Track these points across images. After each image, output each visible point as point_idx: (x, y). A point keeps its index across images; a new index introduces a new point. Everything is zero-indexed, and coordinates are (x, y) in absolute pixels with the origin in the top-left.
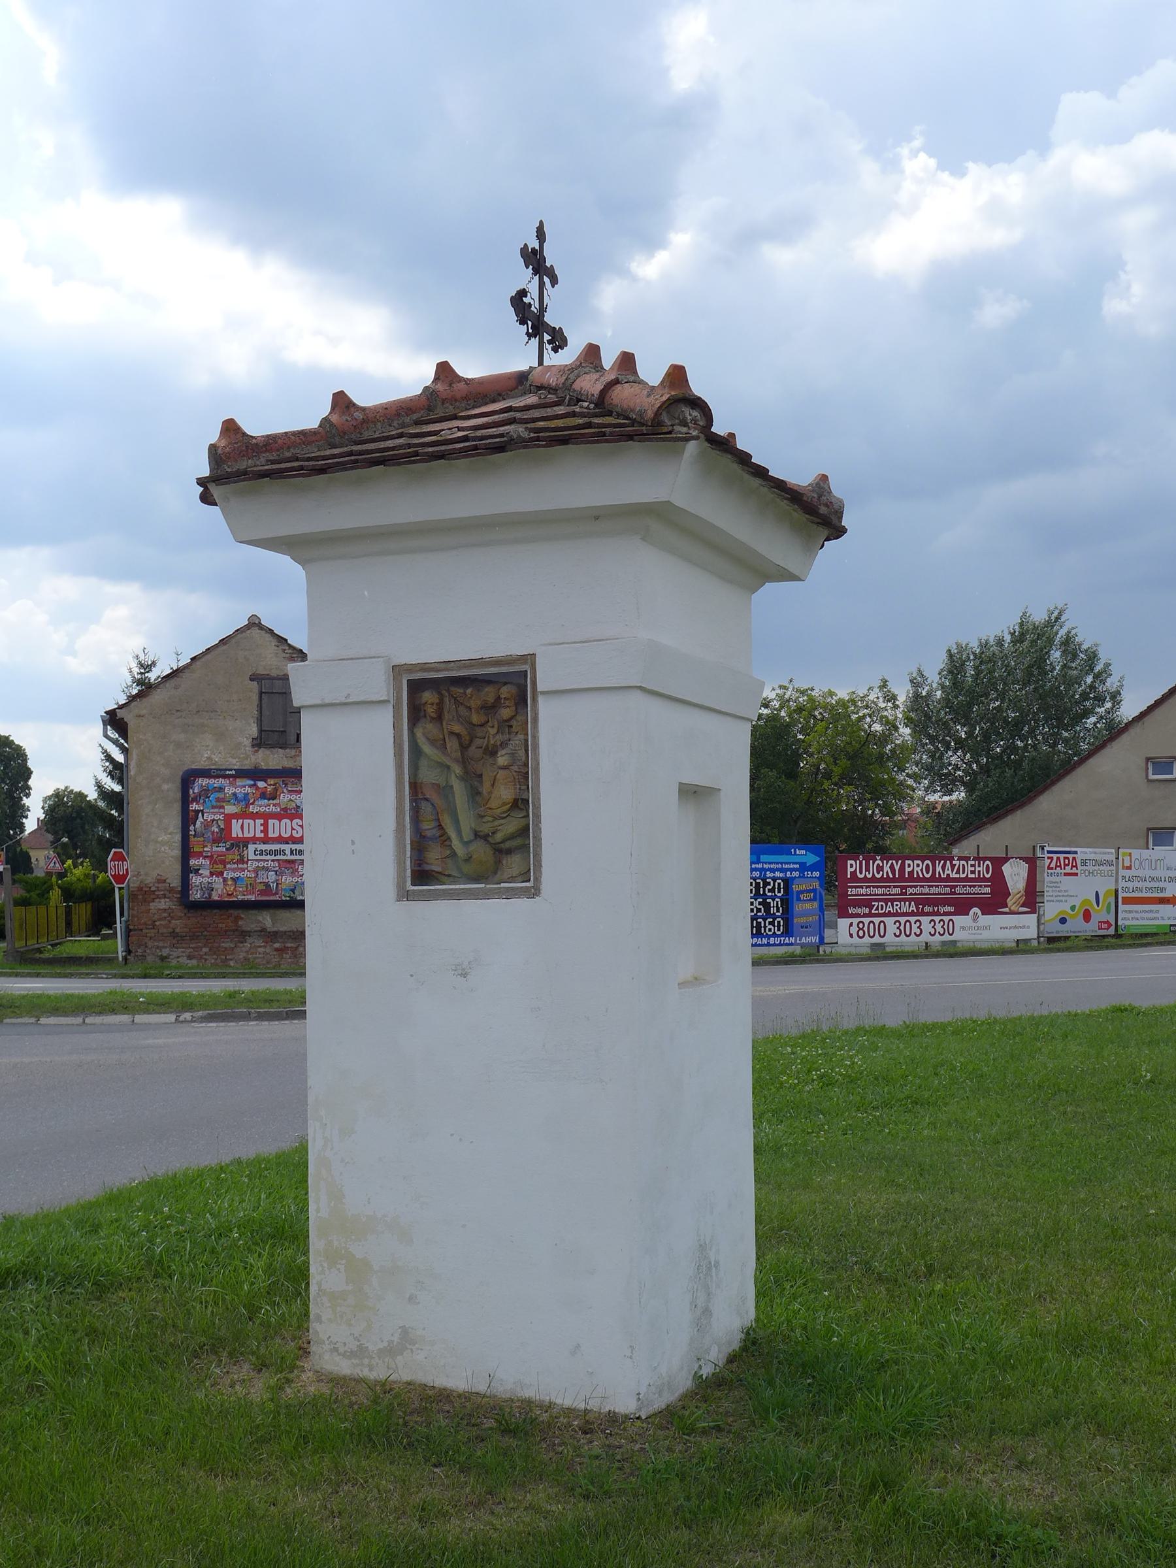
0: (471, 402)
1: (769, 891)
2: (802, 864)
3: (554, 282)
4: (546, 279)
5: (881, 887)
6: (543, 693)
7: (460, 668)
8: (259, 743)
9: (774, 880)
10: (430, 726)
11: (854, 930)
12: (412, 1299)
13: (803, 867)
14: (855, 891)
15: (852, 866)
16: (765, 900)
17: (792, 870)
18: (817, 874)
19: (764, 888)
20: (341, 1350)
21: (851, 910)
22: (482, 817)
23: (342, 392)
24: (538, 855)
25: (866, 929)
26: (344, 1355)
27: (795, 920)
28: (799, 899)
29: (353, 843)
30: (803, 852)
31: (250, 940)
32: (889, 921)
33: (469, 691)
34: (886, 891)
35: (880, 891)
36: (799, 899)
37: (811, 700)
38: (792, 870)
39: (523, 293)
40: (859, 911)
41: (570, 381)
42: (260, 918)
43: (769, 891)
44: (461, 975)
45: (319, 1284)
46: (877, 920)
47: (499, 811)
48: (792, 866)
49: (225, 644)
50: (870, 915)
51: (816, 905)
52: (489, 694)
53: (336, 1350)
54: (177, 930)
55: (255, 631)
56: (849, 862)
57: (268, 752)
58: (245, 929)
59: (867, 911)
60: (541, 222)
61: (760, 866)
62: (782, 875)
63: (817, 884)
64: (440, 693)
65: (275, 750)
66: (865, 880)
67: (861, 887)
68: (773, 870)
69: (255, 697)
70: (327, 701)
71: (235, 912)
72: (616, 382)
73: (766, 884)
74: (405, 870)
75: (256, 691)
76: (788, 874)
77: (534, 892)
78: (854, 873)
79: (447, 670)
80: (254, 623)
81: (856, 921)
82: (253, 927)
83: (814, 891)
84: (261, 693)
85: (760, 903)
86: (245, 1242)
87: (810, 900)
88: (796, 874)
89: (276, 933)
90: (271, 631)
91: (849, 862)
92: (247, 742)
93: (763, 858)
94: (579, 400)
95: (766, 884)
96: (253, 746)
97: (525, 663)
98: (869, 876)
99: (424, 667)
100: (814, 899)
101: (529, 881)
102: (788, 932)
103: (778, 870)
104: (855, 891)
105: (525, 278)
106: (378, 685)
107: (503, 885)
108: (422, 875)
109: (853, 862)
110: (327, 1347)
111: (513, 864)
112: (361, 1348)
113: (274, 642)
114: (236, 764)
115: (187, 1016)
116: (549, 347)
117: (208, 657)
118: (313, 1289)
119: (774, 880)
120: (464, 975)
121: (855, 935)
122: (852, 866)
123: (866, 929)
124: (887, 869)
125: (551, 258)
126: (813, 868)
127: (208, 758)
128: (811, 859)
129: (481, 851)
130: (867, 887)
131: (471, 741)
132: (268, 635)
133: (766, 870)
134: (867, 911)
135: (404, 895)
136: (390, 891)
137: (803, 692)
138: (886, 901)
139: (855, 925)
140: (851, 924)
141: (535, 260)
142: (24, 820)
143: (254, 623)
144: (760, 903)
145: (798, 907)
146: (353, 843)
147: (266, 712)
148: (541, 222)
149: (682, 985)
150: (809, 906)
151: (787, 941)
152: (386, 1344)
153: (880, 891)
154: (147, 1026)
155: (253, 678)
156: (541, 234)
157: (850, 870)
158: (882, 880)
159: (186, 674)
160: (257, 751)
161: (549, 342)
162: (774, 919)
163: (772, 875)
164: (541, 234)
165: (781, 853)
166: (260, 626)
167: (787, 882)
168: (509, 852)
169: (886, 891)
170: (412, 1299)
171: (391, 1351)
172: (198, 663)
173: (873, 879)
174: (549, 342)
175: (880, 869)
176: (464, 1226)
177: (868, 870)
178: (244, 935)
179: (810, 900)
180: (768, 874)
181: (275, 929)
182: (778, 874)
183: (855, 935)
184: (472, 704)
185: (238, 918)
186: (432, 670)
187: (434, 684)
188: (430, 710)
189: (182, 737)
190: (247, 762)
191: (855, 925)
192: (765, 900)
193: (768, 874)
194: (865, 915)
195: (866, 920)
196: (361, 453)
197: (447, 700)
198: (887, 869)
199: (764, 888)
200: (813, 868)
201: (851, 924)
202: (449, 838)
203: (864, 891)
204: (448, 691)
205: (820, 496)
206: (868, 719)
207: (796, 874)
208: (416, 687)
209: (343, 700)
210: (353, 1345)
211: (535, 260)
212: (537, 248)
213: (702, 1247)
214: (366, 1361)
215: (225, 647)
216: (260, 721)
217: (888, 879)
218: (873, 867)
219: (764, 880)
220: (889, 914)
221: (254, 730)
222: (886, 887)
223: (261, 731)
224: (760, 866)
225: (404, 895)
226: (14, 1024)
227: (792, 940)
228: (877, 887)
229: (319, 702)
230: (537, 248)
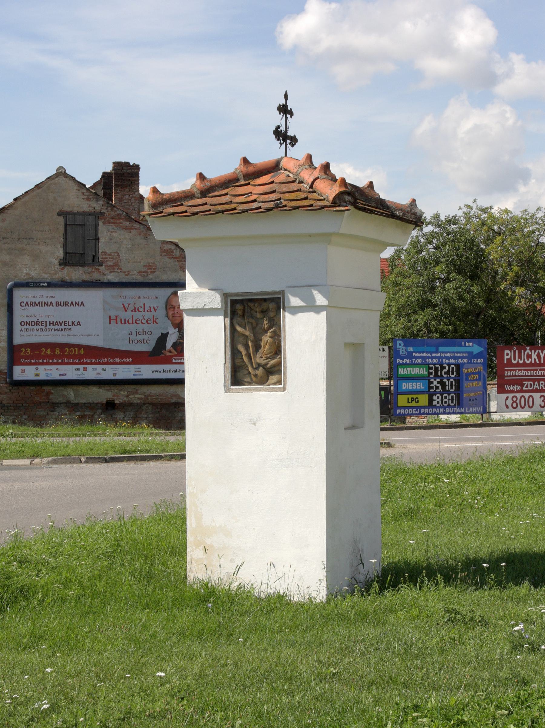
0: (256, 176)
1: (445, 373)
2: (470, 353)
3: (291, 114)
4: (289, 116)
5: (530, 370)
8: (65, 263)
9: (449, 365)
10: (239, 319)
11: (509, 402)
13: (471, 356)
14: (510, 373)
15: (508, 355)
16: (442, 380)
17: (462, 358)
18: (481, 361)
19: (441, 371)
21: (507, 388)
24: (285, 374)
25: (518, 402)
27: (465, 395)
28: (467, 379)
29: (206, 368)
30: (471, 344)
31: (58, 410)
32: (537, 396)
33: (256, 305)
34: (533, 373)
35: (529, 373)
36: (467, 379)
37: (491, 216)
38: (462, 358)
39: (278, 127)
40: (513, 388)
41: (299, 172)
42: (65, 393)
43: (445, 373)
45: (191, 556)
46: (527, 395)
48: (462, 355)
49: (39, 189)
50: (521, 391)
51: (480, 383)
52: (265, 306)
54: (4, 402)
55: (61, 179)
56: (506, 352)
57: (71, 269)
58: (55, 401)
59: (519, 388)
60: (286, 92)
61: (438, 355)
62: (454, 361)
63: (481, 368)
64: (244, 306)
65: (76, 268)
66: (518, 365)
67: (515, 370)
68: (448, 358)
69: (62, 229)
71: (47, 388)
72: (318, 178)
73: (443, 368)
75: (62, 223)
76: (460, 361)
77: (284, 389)
78: (509, 360)
80: (61, 173)
81: (510, 395)
82: (61, 399)
83: (479, 373)
84: (66, 225)
85: (438, 383)
86: (161, 539)
87: (476, 380)
88: (465, 361)
89: (77, 404)
90: (73, 179)
91: (506, 352)
92: (56, 262)
93: (441, 349)
94: (302, 182)
95: (443, 368)
96: (60, 264)
97: (280, 294)
98: (521, 362)
100: (479, 379)
101: (281, 384)
102: (459, 402)
103: (451, 357)
104: (510, 373)
105: (279, 119)
107: (271, 386)
109: (508, 352)
111: (273, 378)
113: (76, 187)
114: (47, 277)
115: (37, 460)
116: (289, 146)
117: (27, 198)
118: (188, 558)
119: (449, 365)
120: (254, 424)
121: (510, 406)
122: (507, 354)
123: (518, 402)
124: (534, 356)
125: (291, 105)
126: (478, 356)
127: (27, 274)
128: (476, 349)
130: (519, 370)
131: (257, 325)
132: (71, 182)
133: (443, 358)
134: (519, 388)
137: (485, 210)
138: (534, 381)
139: (510, 398)
140: (507, 398)
141: (284, 110)
143: (61, 173)
144: (438, 383)
145: (467, 385)
146: (206, 368)
147: (69, 239)
148: (286, 92)
149: (345, 429)
150: (475, 384)
151: (458, 410)
153: (529, 373)
154: (10, 468)
155: (60, 214)
156: (286, 97)
157: (506, 357)
158: (531, 365)
159: (10, 211)
160: (63, 269)
161: (290, 144)
162: (449, 394)
163: (447, 361)
164: (286, 97)
165: (453, 345)
166: (65, 175)
167: (458, 366)
169: (533, 373)
172: (19, 202)
173: (524, 364)
174: (290, 144)
175: (529, 356)
176: (254, 529)
177: (520, 357)
178: (54, 406)
179: (476, 380)
180: (444, 361)
181: (77, 401)
182: (452, 361)
183: (510, 406)
184: (257, 309)
185: (49, 393)
186: (242, 296)
187: (241, 301)
188: (240, 312)
189: (7, 258)
190: (56, 277)
191: (510, 398)
192: (442, 380)
193: (444, 361)
194: (518, 392)
195: (519, 395)
197: (246, 307)
198: (534, 356)
199: (441, 371)
200: (478, 356)
201: (507, 398)
202: (247, 366)
203: (517, 373)
204: (247, 304)
205: (411, 210)
206: (537, 233)
207: (465, 361)
208: (234, 302)
211: (284, 110)
212: (285, 104)
213: (355, 542)
215: (39, 191)
216: (65, 246)
217: (535, 365)
218: (524, 355)
219: (441, 366)
220: (536, 391)
221: (60, 253)
222: (534, 370)
223: (66, 253)
224: (438, 355)
227: (462, 410)
228: (527, 370)
230: (285, 104)
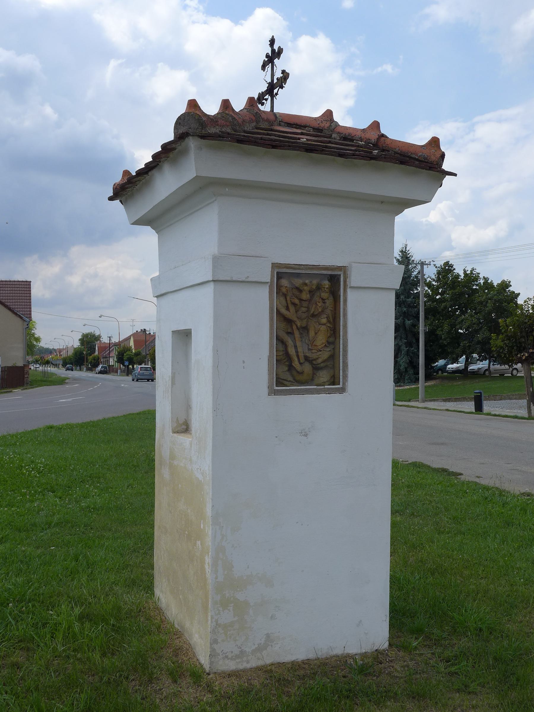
6: (351, 287)
7: (306, 269)
12: (273, 617)
20: (230, 656)
22: (311, 350)
23: (228, 100)
26: (232, 659)
29: (244, 362)
44: (304, 435)
47: (320, 347)
53: (227, 657)
70: (234, 279)
74: (273, 378)
79: (299, 269)
97: (341, 270)
99: (287, 266)
106: (266, 275)
108: (280, 382)
110: (220, 657)
111: (324, 376)
112: (242, 652)
120: (306, 435)
129: (307, 368)
135: (272, 392)
136: (266, 390)
142: (511, 289)
146: (244, 362)
152: (257, 646)
168: (321, 369)
170: (273, 617)
171: (260, 649)
196: (292, 143)
209: (244, 279)
210: (237, 651)
214: (245, 659)
225: (272, 392)
226: (408, 406)
229: (229, 279)
